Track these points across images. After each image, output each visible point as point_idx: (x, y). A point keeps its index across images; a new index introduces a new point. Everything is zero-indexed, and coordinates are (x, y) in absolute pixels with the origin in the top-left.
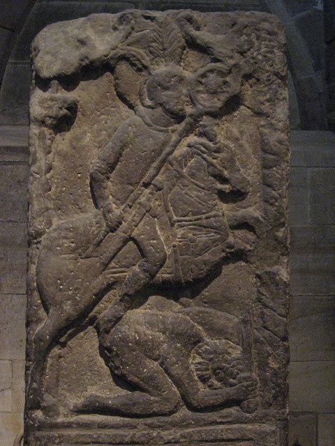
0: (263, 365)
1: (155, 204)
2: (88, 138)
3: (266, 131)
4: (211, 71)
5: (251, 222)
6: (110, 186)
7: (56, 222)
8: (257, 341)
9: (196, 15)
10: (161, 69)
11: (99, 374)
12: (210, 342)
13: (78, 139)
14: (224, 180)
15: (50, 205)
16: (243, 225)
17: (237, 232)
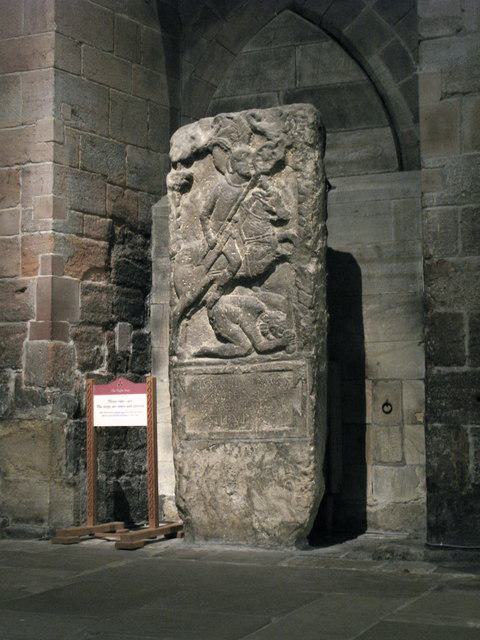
0: (298, 325)
1: (234, 231)
2: (199, 196)
3: (300, 180)
4: (265, 147)
5: (290, 237)
6: (211, 223)
7: (183, 246)
8: (294, 310)
9: (257, 112)
10: (237, 149)
11: (209, 335)
12: (268, 312)
13: (194, 196)
14: (274, 214)
15: (180, 236)
16: (285, 240)
17: (284, 245)
